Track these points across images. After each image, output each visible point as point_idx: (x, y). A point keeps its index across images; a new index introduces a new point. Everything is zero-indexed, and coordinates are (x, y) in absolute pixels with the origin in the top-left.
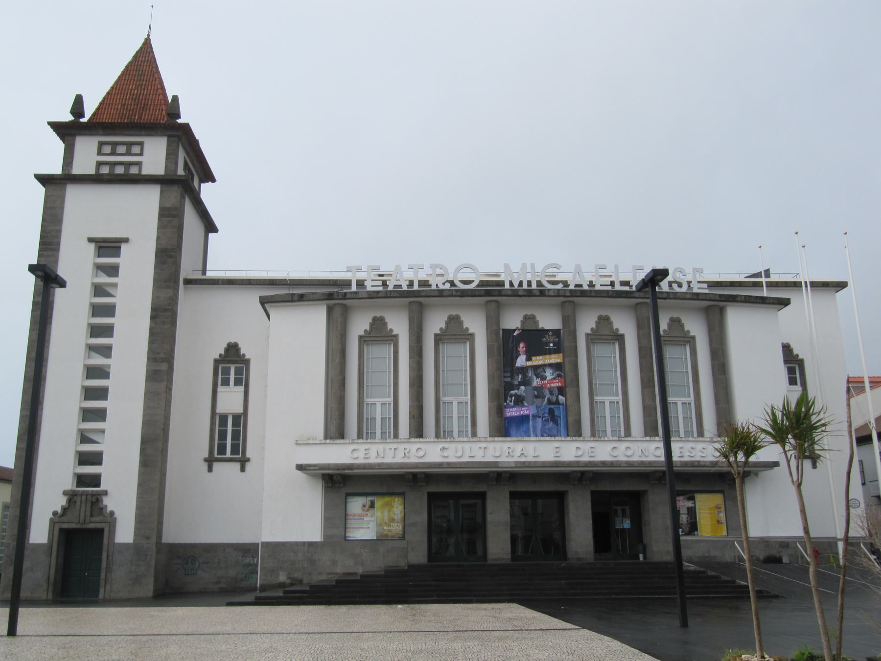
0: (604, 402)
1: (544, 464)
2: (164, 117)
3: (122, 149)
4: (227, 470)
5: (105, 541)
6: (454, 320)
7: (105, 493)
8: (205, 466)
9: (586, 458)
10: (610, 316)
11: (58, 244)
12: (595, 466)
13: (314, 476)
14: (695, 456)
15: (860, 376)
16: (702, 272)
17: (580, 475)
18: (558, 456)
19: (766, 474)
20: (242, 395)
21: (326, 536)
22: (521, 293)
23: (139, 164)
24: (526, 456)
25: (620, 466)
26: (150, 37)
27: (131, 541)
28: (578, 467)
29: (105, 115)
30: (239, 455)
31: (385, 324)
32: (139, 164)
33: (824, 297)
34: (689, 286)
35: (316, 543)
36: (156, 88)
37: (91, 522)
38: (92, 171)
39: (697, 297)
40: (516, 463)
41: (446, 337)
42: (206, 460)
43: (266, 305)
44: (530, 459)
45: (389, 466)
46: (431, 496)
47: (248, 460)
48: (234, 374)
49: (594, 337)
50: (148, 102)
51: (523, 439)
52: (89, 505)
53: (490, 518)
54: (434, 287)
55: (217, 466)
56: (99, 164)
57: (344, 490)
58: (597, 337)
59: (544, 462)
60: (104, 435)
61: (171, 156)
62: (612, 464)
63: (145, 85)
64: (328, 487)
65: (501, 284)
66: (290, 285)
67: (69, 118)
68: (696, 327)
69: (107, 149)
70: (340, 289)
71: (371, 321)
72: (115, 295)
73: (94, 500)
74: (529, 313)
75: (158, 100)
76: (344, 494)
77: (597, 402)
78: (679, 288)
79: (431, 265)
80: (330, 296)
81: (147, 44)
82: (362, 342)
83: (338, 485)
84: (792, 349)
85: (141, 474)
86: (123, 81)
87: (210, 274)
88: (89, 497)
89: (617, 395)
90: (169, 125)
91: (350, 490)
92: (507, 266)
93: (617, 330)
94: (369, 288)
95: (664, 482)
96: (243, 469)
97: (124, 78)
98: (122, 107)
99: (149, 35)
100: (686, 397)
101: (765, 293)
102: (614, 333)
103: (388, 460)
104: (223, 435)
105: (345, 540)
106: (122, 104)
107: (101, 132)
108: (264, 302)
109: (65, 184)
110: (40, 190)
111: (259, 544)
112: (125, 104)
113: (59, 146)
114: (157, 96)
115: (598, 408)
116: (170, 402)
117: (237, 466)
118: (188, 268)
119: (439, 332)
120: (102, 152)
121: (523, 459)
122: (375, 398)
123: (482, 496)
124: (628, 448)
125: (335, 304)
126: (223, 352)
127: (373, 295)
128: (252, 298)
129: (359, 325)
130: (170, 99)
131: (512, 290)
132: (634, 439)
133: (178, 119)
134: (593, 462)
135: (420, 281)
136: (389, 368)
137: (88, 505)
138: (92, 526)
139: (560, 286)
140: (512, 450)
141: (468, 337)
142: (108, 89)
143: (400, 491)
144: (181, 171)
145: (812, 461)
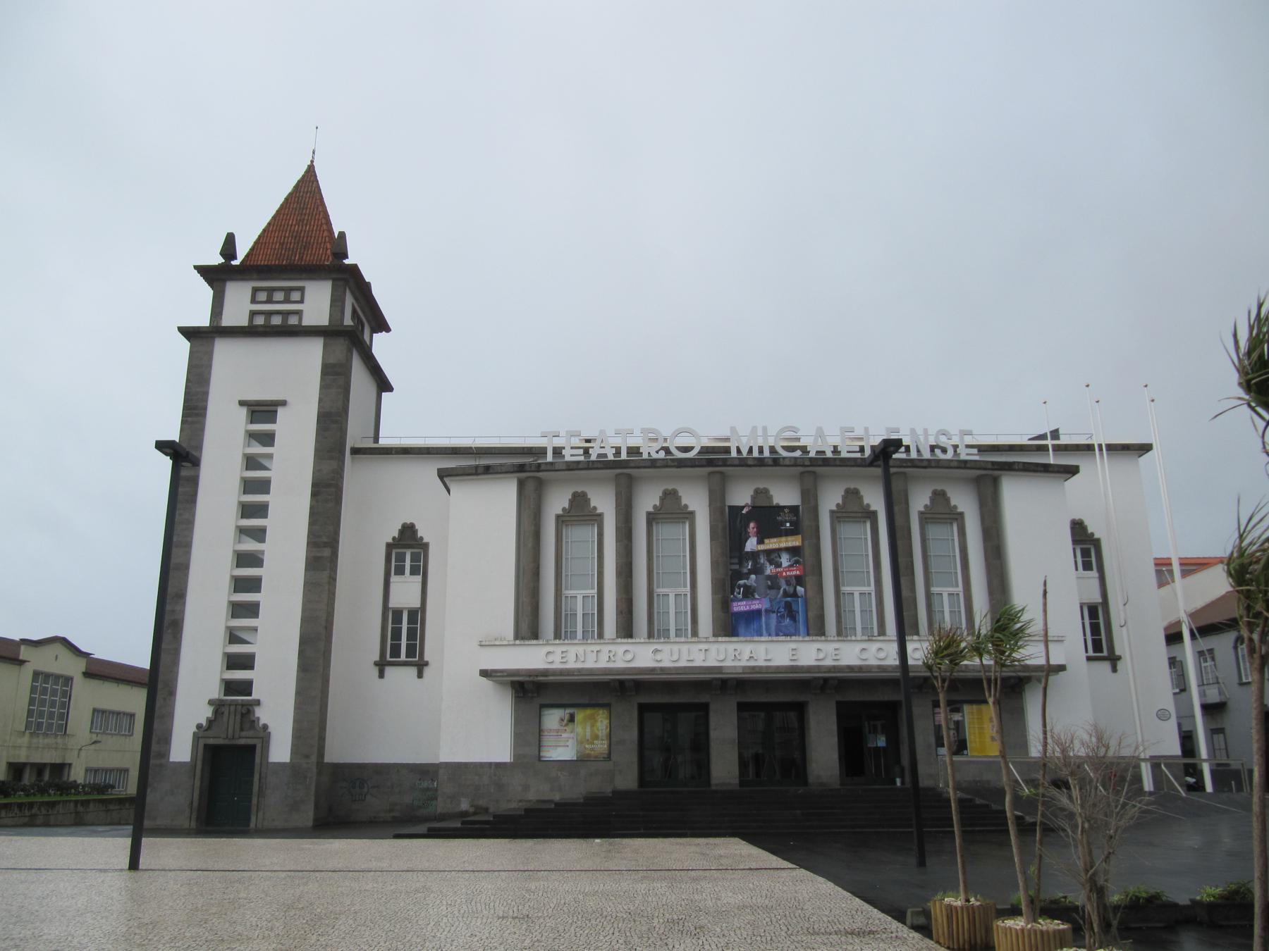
0: (668, 595)
1: (778, 669)
3: (279, 296)
4: (401, 676)
5: (257, 760)
6: (670, 496)
7: (258, 703)
8: (375, 671)
9: (829, 662)
11: (205, 408)
13: (502, 683)
21: (516, 756)
22: (750, 462)
23: (299, 313)
31: (587, 501)
32: (299, 313)
33: (1124, 464)
34: (955, 451)
37: (240, 738)
38: (243, 321)
39: (964, 464)
40: (744, 668)
42: (376, 664)
44: (761, 663)
47: (427, 664)
52: (238, 717)
53: (714, 734)
54: (645, 456)
56: (253, 314)
61: (337, 303)
64: (518, 697)
66: (476, 454)
69: (262, 296)
70: (536, 458)
75: (322, 237)
77: (844, 593)
80: (521, 468)
84: (417, 530)
85: (299, 680)
88: (239, 707)
93: (868, 505)
94: (568, 458)
96: (420, 675)
99: (312, 162)
101: (1051, 459)
104: (397, 634)
106: (280, 243)
108: (443, 475)
109: (213, 338)
110: (185, 345)
112: (283, 243)
113: (207, 292)
116: (334, 594)
118: (356, 434)
120: (257, 300)
121: (752, 663)
124: (880, 649)
127: (573, 467)
128: (428, 471)
129: (557, 502)
134: (838, 666)
136: (593, 553)
137: (237, 717)
138: (242, 742)
139: (798, 454)
141: (687, 516)
144: (348, 321)
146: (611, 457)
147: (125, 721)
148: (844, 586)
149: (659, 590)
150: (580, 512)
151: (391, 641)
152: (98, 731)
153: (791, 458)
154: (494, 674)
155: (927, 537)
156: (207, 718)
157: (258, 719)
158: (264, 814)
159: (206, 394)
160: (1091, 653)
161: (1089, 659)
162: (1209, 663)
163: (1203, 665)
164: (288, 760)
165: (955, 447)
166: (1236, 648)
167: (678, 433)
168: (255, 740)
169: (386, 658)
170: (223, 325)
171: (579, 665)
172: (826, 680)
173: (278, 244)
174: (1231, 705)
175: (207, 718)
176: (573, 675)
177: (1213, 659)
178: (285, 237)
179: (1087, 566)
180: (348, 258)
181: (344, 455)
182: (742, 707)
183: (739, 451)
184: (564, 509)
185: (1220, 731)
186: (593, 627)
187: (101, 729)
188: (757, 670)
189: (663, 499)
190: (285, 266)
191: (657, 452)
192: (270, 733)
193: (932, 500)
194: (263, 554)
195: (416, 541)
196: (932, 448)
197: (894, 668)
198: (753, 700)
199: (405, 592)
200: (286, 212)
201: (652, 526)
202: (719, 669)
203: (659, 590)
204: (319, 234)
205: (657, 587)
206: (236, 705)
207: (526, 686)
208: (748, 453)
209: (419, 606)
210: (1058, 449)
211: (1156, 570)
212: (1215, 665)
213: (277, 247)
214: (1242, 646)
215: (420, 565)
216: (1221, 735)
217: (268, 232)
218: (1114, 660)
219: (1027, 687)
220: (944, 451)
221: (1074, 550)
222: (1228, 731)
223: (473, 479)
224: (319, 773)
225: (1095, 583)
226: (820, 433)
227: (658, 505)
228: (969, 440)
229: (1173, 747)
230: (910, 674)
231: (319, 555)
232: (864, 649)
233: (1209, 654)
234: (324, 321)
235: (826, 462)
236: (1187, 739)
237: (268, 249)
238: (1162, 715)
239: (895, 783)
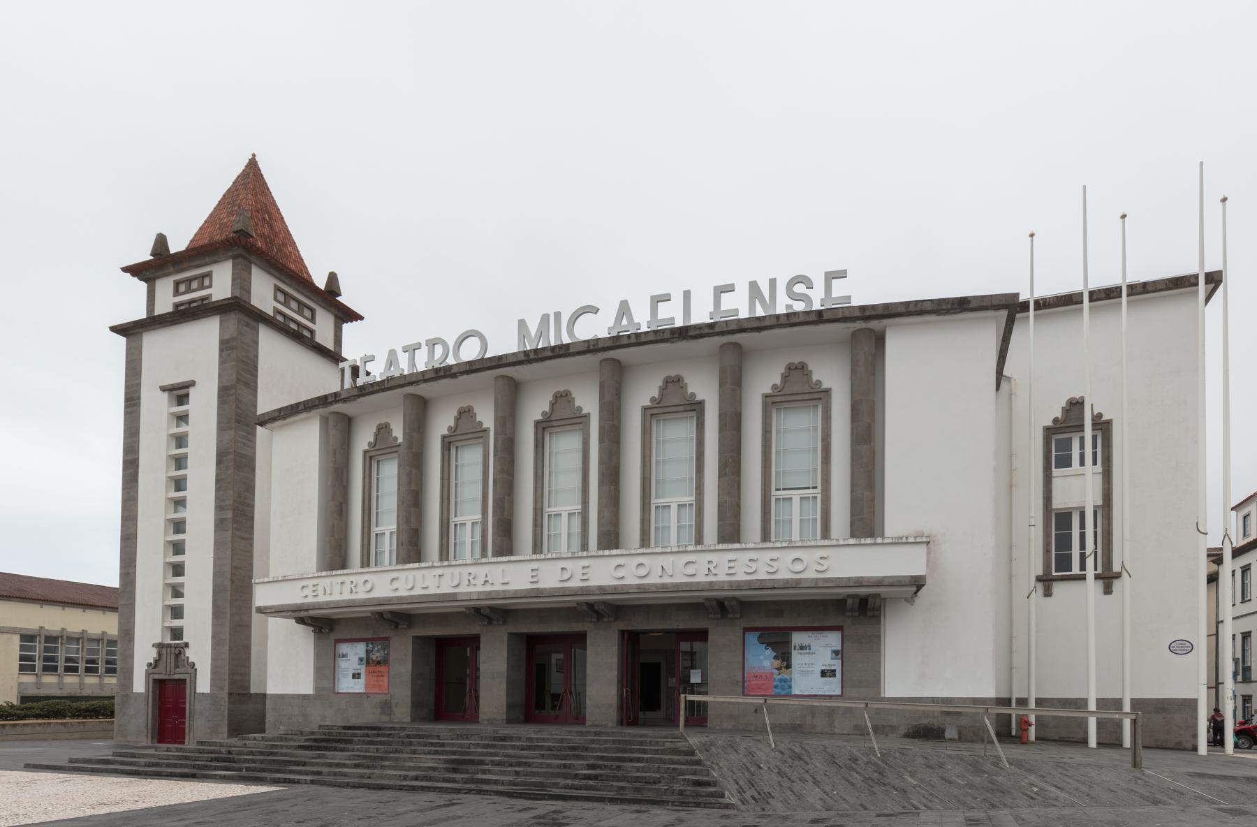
0: (791, 498)
6: (798, 371)
7: (187, 645)
9: (576, 583)
10: (808, 364)
18: (587, 580)
21: (317, 688)
24: (492, 584)
35: (309, 695)
37: (175, 674)
40: (479, 593)
42: (1039, 579)
44: (498, 587)
48: (512, 557)
51: (538, 558)
55: (1058, 588)
57: (334, 636)
76: (333, 641)
79: (404, 347)
85: (214, 625)
88: (173, 649)
91: (339, 637)
103: (336, 597)
109: (141, 333)
119: (447, 433)
121: (488, 588)
124: (640, 565)
126: (1059, 415)
132: (834, 543)
138: (176, 677)
140: (714, 565)
143: (385, 636)
149: (659, 501)
151: (1056, 551)
158: (194, 734)
171: (666, 580)
188: (770, 585)
189: (457, 419)
202: (452, 597)
203: (659, 501)
205: (656, 498)
227: (657, 397)
231: (224, 517)
232: (393, 579)
239: (170, 707)
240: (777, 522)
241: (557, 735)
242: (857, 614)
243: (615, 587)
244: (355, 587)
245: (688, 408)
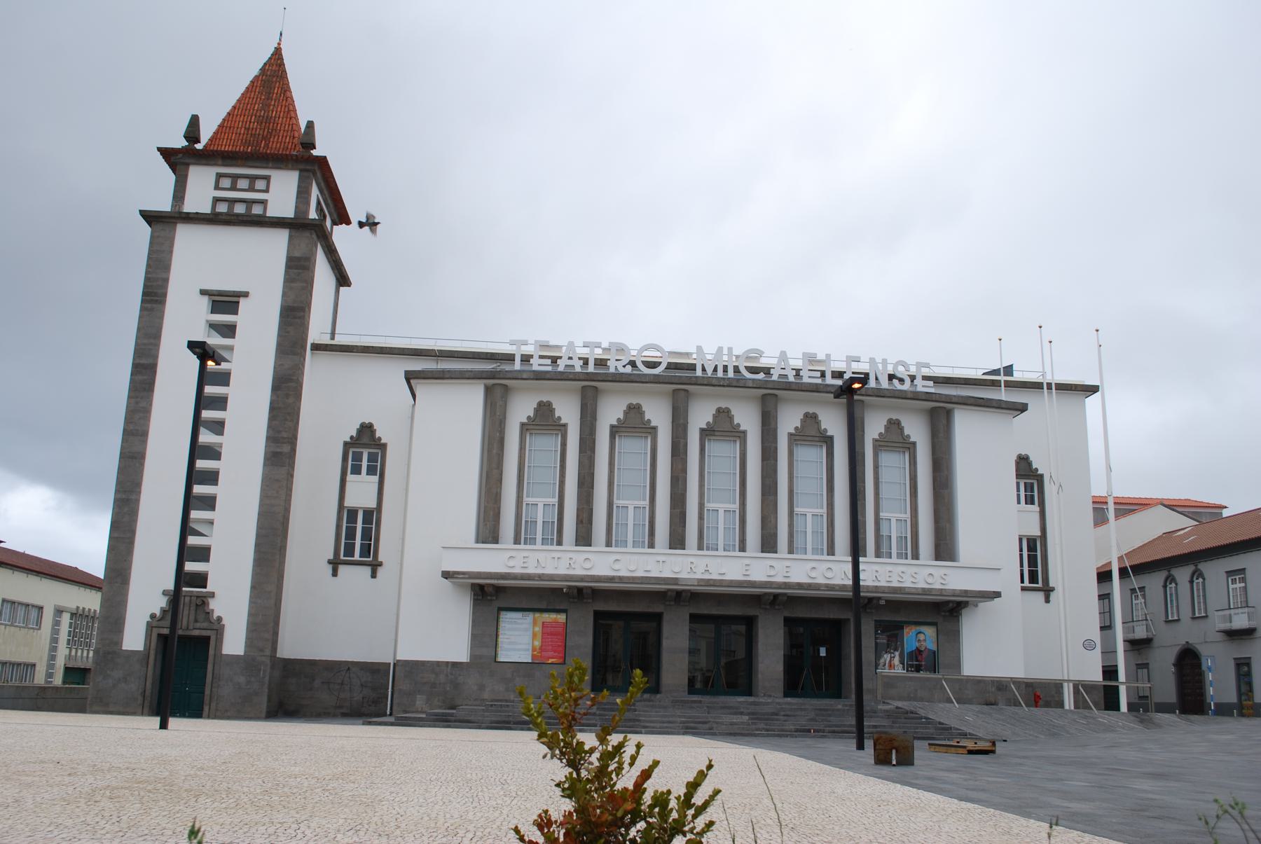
0: (627, 507)
1: (732, 583)
2: (295, 146)
3: (243, 183)
4: (354, 576)
5: (211, 652)
7: (212, 595)
8: (329, 569)
9: (779, 579)
11: (165, 295)
12: (790, 588)
13: (461, 586)
14: (777, 574)
15: (1118, 496)
16: (859, 361)
17: (772, 598)
19: (985, 606)
20: (1037, 517)
21: (473, 656)
22: (714, 382)
23: (264, 203)
25: (819, 590)
26: (281, 46)
27: (242, 653)
28: (771, 588)
29: (225, 140)
30: (370, 557)
31: (552, 411)
32: (264, 203)
33: (1070, 399)
34: (912, 381)
36: (287, 110)
38: (206, 209)
39: (916, 396)
40: (700, 580)
41: (624, 429)
42: (330, 562)
43: (412, 381)
45: (551, 578)
46: (598, 615)
47: (380, 564)
49: (798, 438)
50: (277, 127)
52: (193, 608)
53: (666, 643)
54: (612, 370)
55: (342, 569)
56: (216, 200)
57: (497, 604)
58: (886, 444)
59: (731, 581)
60: (212, 528)
61: (303, 194)
62: (809, 586)
63: (274, 105)
64: (477, 600)
65: (692, 367)
66: (439, 356)
67: (181, 143)
68: (916, 430)
69: (226, 183)
70: (499, 364)
71: (714, 413)
72: (230, 360)
73: (199, 602)
74: (723, 405)
75: (289, 125)
77: (797, 514)
78: (900, 386)
80: (491, 375)
81: (278, 53)
82: (524, 430)
83: (489, 598)
84: (375, 430)
85: (256, 575)
86: (247, 99)
87: (340, 340)
89: (645, 500)
90: (302, 158)
92: (699, 348)
93: (826, 430)
94: (535, 368)
95: (955, 614)
96: (374, 575)
97: (248, 95)
98: (246, 132)
99: (279, 44)
100: (730, 503)
101: (1003, 395)
102: (821, 433)
104: (351, 534)
105: (495, 661)
106: (245, 128)
107: (220, 162)
108: (410, 377)
109: (176, 223)
110: (146, 230)
111: (390, 664)
112: (249, 129)
113: (170, 177)
114: (288, 119)
115: (798, 522)
116: (291, 490)
117: (368, 570)
118: (317, 331)
119: (616, 423)
120: (220, 186)
121: (707, 577)
122: (537, 497)
123: (657, 618)
125: (494, 385)
126: (354, 434)
127: (539, 376)
128: (395, 371)
129: (521, 409)
130: (303, 126)
131: (703, 377)
133: (312, 150)
135: (596, 359)
136: (555, 463)
137: (192, 608)
138: (196, 633)
139: (761, 376)
140: (573, 561)
141: (649, 430)
142: (228, 108)
144: (313, 215)
145: (1045, 594)
146: (578, 369)
147: (34, 613)
148: (798, 507)
149: (621, 502)
150: (544, 419)
152: (7, 623)
153: (753, 380)
154: (456, 576)
155: (880, 464)
156: (161, 608)
157: (213, 610)
158: (217, 704)
159: (166, 280)
160: (1027, 584)
161: (1023, 589)
162: (1141, 600)
163: (1134, 602)
164: (242, 653)
165: (913, 378)
166: (1165, 587)
167: (647, 347)
168: (209, 631)
169: (339, 556)
170: (185, 211)
172: (776, 596)
173: (243, 129)
174: (1156, 643)
175: (161, 608)
176: (534, 580)
177: (1144, 597)
178: (250, 122)
179: (1029, 500)
180: (315, 148)
181: (305, 351)
182: (694, 618)
183: (704, 369)
184: (529, 418)
185: (1145, 666)
186: (553, 535)
187: (9, 621)
188: (712, 583)
190: (250, 153)
191: (624, 366)
192: (224, 625)
193: (887, 428)
194: (221, 447)
195: (374, 441)
196: (891, 377)
197: (843, 588)
198: (706, 612)
199: (361, 492)
200: (252, 96)
201: (615, 438)
203: (621, 502)
204: (286, 121)
206: (191, 596)
207: (486, 588)
208: (713, 371)
209: (375, 506)
210: (1009, 385)
211: (1115, 509)
212: (1145, 602)
213: (242, 132)
214: (1171, 586)
215: (377, 465)
216: (1146, 670)
217: (233, 115)
218: (1047, 591)
219: (964, 612)
220: (901, 380)
221: (1018, 484)
222: (1151, 666)
223: (432, 383)
224: (273, 667)
225: (1036, 518)
226: (783, 357)
228: (926, 372)
229: (1096, 676)
230: (862, 594)
231: (278, 450)
233: (1140, 592)
234: (288, 212)
235: (788, 387)
236: (1110, 672)
237: (233, 133)
238: (1088, 645)
240: (708, 527)
241: (466, 705)
242: (576, 600)
243: (827, 585)
244: (574, 563)
245: (822, 439)
